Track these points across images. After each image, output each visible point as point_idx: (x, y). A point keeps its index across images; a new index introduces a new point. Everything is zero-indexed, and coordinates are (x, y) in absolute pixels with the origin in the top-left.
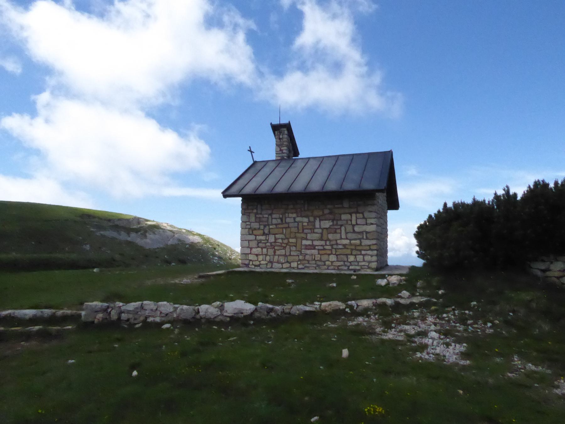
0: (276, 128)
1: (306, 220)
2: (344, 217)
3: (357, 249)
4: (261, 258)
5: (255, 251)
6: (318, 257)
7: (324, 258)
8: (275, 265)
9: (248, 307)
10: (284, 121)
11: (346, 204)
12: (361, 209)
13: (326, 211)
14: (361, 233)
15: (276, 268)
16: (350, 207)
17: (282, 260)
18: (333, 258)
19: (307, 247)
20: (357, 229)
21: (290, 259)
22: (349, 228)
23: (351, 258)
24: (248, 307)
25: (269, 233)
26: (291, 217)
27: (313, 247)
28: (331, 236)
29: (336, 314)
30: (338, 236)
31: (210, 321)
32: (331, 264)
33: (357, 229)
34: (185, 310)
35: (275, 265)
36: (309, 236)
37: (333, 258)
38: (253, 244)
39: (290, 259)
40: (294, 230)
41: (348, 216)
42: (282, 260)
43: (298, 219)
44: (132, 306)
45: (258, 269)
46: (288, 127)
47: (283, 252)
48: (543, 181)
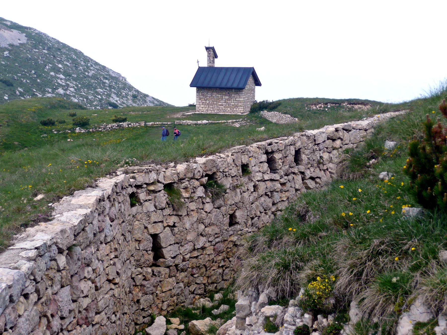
0: (207, 49)
1: (220, 96)
2: (233, 95)
3: (236, 106)
4: (204, 108)
5: (201, 106)
6: (224, 109)
7: (226, 109)
8: (209, 111)
9: (207, 122)
10: (211, 46)
11: (233, 91)
12: (238, 93)
13: (227, 93)
14: (238, 101)
15: (209, 112)
16: (235, 92)
17: (211, 109)
18: (229, 109)
19: (220, 105)
20: (237, 99)
21: (214, 109)
22: (234, 99)
23: (235, 109)
24: (207, 122)
25: (207, 100)
26: (214, 94)
27: (222, 105)
28: (228, 102)
29: (224, 123)
30: (231, 102)
31: (200, 124)
32: (228, 112)
33: (237, 99)
34: (195, 122)
35: (209, 111)
36: (221, 101)
37: (229, 109)
38: (201, 103)
39: (214, 109)
40: (216, 99)
41: (234, 95)
42: (211, 109)
43: (217, 95)
44: (184, 121)
45: (203, 113)
46: (213, 49)
47: (212, 107)
48: (267, 101)
